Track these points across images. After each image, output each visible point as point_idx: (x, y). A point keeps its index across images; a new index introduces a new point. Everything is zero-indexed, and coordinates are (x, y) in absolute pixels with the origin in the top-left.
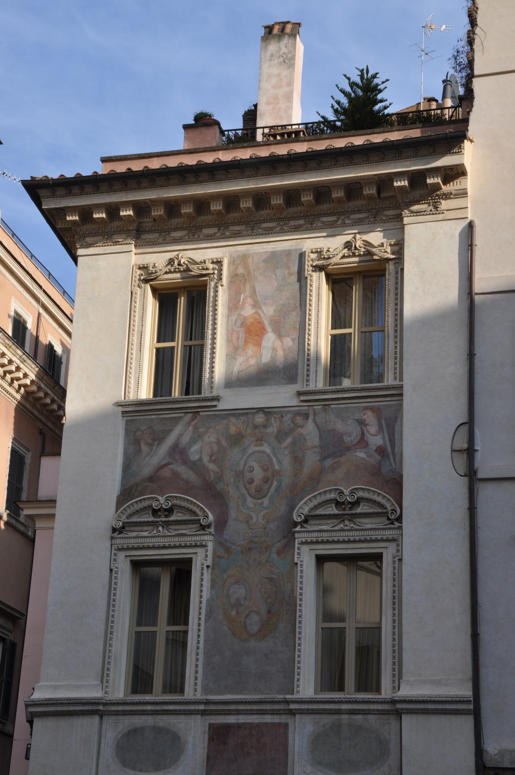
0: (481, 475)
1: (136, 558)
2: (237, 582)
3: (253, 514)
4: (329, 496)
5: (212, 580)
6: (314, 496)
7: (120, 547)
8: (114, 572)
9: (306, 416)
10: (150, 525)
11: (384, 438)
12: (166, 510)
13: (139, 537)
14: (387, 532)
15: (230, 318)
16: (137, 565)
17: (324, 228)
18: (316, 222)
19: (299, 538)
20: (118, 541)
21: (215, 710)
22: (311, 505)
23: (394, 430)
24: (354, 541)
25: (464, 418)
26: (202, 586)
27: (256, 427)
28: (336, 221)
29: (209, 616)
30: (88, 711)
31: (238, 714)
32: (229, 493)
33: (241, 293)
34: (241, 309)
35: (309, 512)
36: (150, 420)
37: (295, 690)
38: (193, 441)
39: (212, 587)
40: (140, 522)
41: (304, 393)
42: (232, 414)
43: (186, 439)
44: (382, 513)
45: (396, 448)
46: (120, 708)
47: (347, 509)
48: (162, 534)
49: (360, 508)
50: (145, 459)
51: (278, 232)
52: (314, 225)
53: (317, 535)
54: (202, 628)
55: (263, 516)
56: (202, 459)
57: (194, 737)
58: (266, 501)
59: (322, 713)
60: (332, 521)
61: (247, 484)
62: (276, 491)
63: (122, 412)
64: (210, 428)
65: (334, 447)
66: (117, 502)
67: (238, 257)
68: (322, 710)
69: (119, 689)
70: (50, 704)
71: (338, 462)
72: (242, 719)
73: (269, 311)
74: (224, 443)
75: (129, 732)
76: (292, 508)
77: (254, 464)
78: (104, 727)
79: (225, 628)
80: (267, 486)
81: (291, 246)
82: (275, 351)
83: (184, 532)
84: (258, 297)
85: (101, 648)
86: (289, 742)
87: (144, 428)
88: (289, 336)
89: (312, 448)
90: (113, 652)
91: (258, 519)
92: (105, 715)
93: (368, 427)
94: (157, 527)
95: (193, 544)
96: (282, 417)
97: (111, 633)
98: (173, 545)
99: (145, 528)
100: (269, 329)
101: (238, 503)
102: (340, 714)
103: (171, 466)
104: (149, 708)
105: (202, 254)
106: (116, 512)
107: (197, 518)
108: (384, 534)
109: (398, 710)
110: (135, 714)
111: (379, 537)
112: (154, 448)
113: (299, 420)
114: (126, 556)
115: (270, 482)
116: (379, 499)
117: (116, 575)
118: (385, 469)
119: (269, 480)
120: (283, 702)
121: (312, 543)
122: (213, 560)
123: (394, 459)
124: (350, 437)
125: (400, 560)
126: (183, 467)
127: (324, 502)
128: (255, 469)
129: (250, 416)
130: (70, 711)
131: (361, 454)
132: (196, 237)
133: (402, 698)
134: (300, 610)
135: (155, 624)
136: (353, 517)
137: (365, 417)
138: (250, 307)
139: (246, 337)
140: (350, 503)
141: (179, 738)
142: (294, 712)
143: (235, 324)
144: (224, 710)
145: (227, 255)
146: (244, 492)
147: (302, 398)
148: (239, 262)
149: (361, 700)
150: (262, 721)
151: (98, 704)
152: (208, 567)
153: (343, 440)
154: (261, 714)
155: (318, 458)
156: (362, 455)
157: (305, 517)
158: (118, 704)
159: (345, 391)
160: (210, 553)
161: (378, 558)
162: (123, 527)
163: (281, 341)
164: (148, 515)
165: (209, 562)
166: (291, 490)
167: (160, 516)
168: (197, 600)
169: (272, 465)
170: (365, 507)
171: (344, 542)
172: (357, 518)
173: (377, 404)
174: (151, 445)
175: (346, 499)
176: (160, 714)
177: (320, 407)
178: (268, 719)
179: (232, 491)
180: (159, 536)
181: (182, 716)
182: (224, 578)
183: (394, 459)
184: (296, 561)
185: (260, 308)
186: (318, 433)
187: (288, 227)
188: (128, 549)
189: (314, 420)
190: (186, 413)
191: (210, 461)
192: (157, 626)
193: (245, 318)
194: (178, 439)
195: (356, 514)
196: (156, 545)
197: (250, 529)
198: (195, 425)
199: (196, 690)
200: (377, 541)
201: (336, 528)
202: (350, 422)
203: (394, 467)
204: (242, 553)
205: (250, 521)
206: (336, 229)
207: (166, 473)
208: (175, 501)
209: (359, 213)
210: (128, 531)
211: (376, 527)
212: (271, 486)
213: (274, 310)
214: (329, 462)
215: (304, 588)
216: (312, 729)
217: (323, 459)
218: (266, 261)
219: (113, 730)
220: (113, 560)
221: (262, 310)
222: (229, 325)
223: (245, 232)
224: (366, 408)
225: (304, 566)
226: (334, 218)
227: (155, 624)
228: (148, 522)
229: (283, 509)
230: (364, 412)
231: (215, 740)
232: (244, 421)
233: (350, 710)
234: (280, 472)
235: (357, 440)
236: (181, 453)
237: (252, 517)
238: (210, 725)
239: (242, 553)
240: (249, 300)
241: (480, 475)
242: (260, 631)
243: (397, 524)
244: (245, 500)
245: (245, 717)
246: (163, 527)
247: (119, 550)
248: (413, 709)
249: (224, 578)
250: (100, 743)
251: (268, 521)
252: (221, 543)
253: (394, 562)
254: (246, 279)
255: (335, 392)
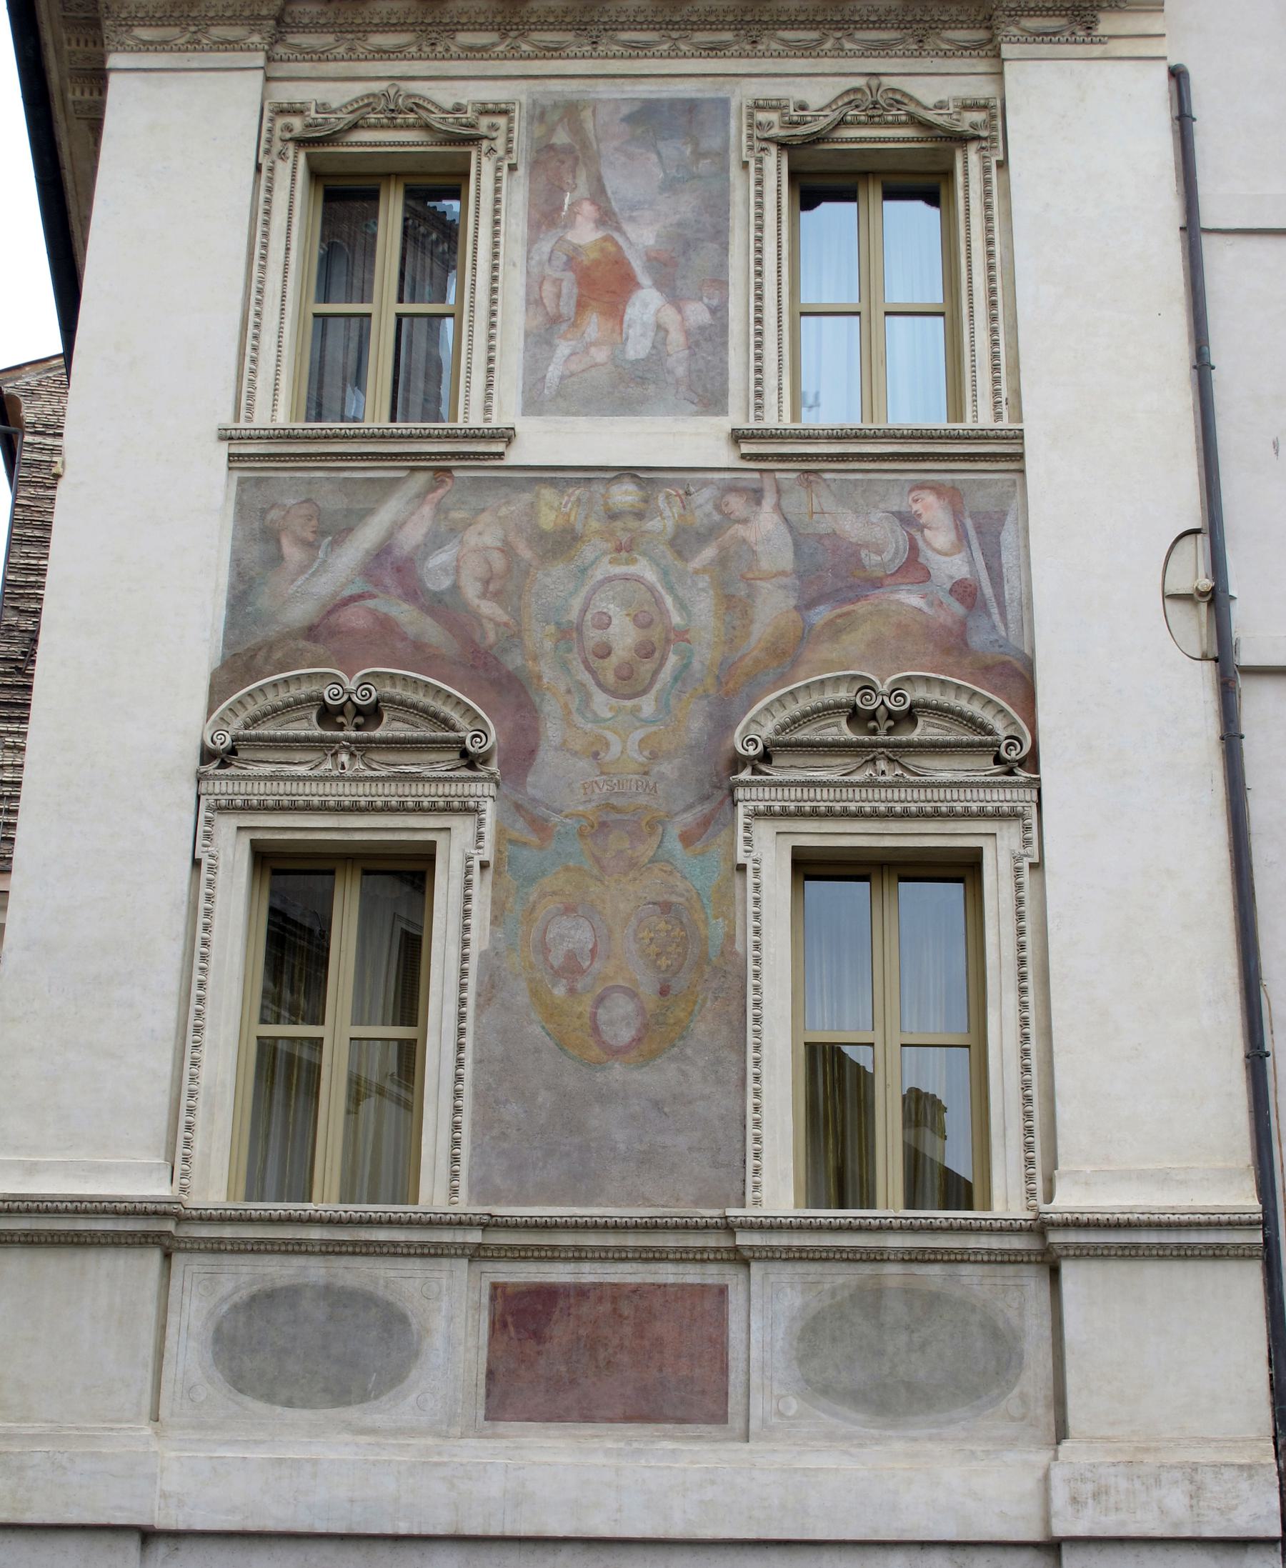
0: (1246, 657)
1: (268, 836)
2: (568, 910)
3: (609, 735)
4: (831, 696)
5: (494, 902)
6: (791, 692)
7: (223, 803)
8: (204, 867)
9: (756, 496)
10: (313, 749)
11: (971, 562)
12: (359, 711)
13: (282, 778)
14: (996, 795)
15: (536, 246)
16: (266, 859)
17: (787, 56)
18: (765, 40)
19: (750, 798)
20: (220, 787)
21: (512, 1248)
22: (783, 716)
23: (998, 544)
24: (906, 815)
25: (1194, 519)
26: (466, 914)
27: (613, 516)
28: (820, 42)
29: (487, 996)
30: (132, 1234)
31: (579, 1259)
32: (540, 678)
33: (563, 191)
34: (565, 227)
35: (777, 733)
36: (310, 482)
37: (749, 1197)
38: (435, 542)
39: (495, 920)
40: (285, 739)
41: (753, 437)
42: (546, 479)
43: (413, 535)
44: (981, 745)
45: (1006, 587)
46: (228, 1232)
47: (879, 728)
48: (348, 773)
49: (918, 731)
50: (293, 581)
51: (665, 54)
52: (760, 47)
53: (799, 794)
54: (469, 1025)
55: (641, 741)
56: (459, 587)
57: (451, 1319)
58: (647, 705)
59: (827, 1259)
60: (839, 761)
61: (591, 658)
62: (676, 679)
63: (230, 455)
64: (483, 510)
65: (834, 578)
66: (211, 686)
67: (555, 105)
68: (827, 1249)
69: (213, 1184)
70: (18, 1211)
71: (848, 614)
72: (589, 1273)
73: (641, 238)
74: (525, 553)
75: (253, 1298)
76: (724, 725)
77: (612, 609)
78: (175, 1283)
79: (537, 1030)
80: (647, 667)
81: (698, 91)
82: (662, 334)
83: (413, 769)
84: (613, 203)
85: (167, 1069)
86: (731, 1335)
87: (293, 502)
88: (701, 299)
89: (775, 576)
90: (203, 1080)
91: (625, 748)
92: (180, 1250)
93: (926, 532)
94: (335, 755)
95: (441, 804)
96: (688, 493)
97: (198, 1030)
98: (379, 804)
99: (298, 757)
100: (644, 279)
101: (566, 705)
102: (882, 1260)
103: (370, 603)
104: (316, 1234)
105: (454, 85)
106: (210, 711)
107: (452, 734)
108: (988, 798)
109: (1046, 1250)
110: (273, 1252)
111: (974, 807)
112: (321, 554)
113: (737, 504)
114: (239, 828)
115: (657, 655)
116: (974, 709)
117: (211, 876)
118: (978, 640)
119: (653, 651)
120: (716, 1227)
121: (785, 814)
122: (499, 851)
123: (1003, 614)
124: (879, 553)
125: (1037, 867)
126: (405, 606)
127: (816, 711)
128: (615, 621)
129: (598, 488)
130: (78, 1233)
131: (911, 599)
132: (439, 49)
133: (1069, 1216)
134: (757, 988)
135: (317, 1018)
136: (896, 754)
137: (916, 507)
138: (592, 225)
139: (580, 296)
140: (891, 715)
141: (403, 1319)
142: (748, 1254)
143: (550, 260)
144: (540, 1248)
145: (523, 99)
146: (586, 677)
147: (746, 448)
148: (556, 118)
149: (945, 1224)
150: (650, 1279)
151: (165, 1215)
152: (484, 866)
153: (860, 560)
154: (647, 1260)
155: (792, 602)
156: (914, 600)
157: (765, 748)
158: (223, 1220)
159: (865, 437)
160: (489, 829)
161: (964, 868)
162: (233, 751)
163: (680, 311)
164: (305, 724)
165: (488, 854)
166: (718, 677)
167: (341, 727)
168: (454, 952)
169: (663, 612)
170: (930, 730)
171: (875, 815)
172: (909, 754)
173: (949, 476)
174: (311, 546)
175: (883, 703)
176: (347, 1253)
177: (794, 475)
178: (668, 1274)
179: (548, 673)
180: (341, 778)
181: (412, 1259)
182: (531, 899)
183: (1003, 614)
184: (740, 860)
185: (619, 229)
186: (789, 540)
187: (692, 44)
188: (247, 808)
189: (778, 507)
190: (413, 469)
191: (483, 595)
192: (323, 1023)
193: (576, 248)
194: (390, 534)
195: (909, 745)
196: (332, 801)
197: (602, 773)
198: (439, 502)
199: (454, 1191)
200: (967, 815)
201: (856, 778)
202: (876, 516)
203: (1004, 634)
204: (581, 834)
205: (602, 754)
206: (818, 60)
207: (355, 618)
208: (388, 689)
209: (879, 28)
210: (247, 761)
211: (966, 779)
212: (661, 665)
213: (658, 236)
214: (822, 614)
215: (763, 932)
216: (798, 1302)
217: (807, 605)
218: (631, 119)
219: (205, 1292)
220: (200, 834)
221: (623, 233)
222: (533, 263)
223: (573, 48)
224: (921, 486)
225: (763, 874)
226: (814, 35)
227: (317, 1018)
228: (308, 739)
229: (697, 726)
230: (913, 494)
231: (512, 1329)
232: (579, 500)
233: (909, 1251)
234: (687, 631)
235: (898, 563)
236: (399, 570)
237: (607, 745)
238: (495, 1286)
239: (581, 834)
240: (588, 209)
241: (1246, 657)
242: (638, 1040)
243: (1023, 775)
244: (587, 699)
245: (597, 1267)
246: (352, 755)
247: (220, 809)
248: (1096, 1246)
249: (531, 899)
250: (162, 1328)
251: (654, 756)
252: (518, 807)
253: (1018, 870)
254: (577, 159)
255: (838, 437)
